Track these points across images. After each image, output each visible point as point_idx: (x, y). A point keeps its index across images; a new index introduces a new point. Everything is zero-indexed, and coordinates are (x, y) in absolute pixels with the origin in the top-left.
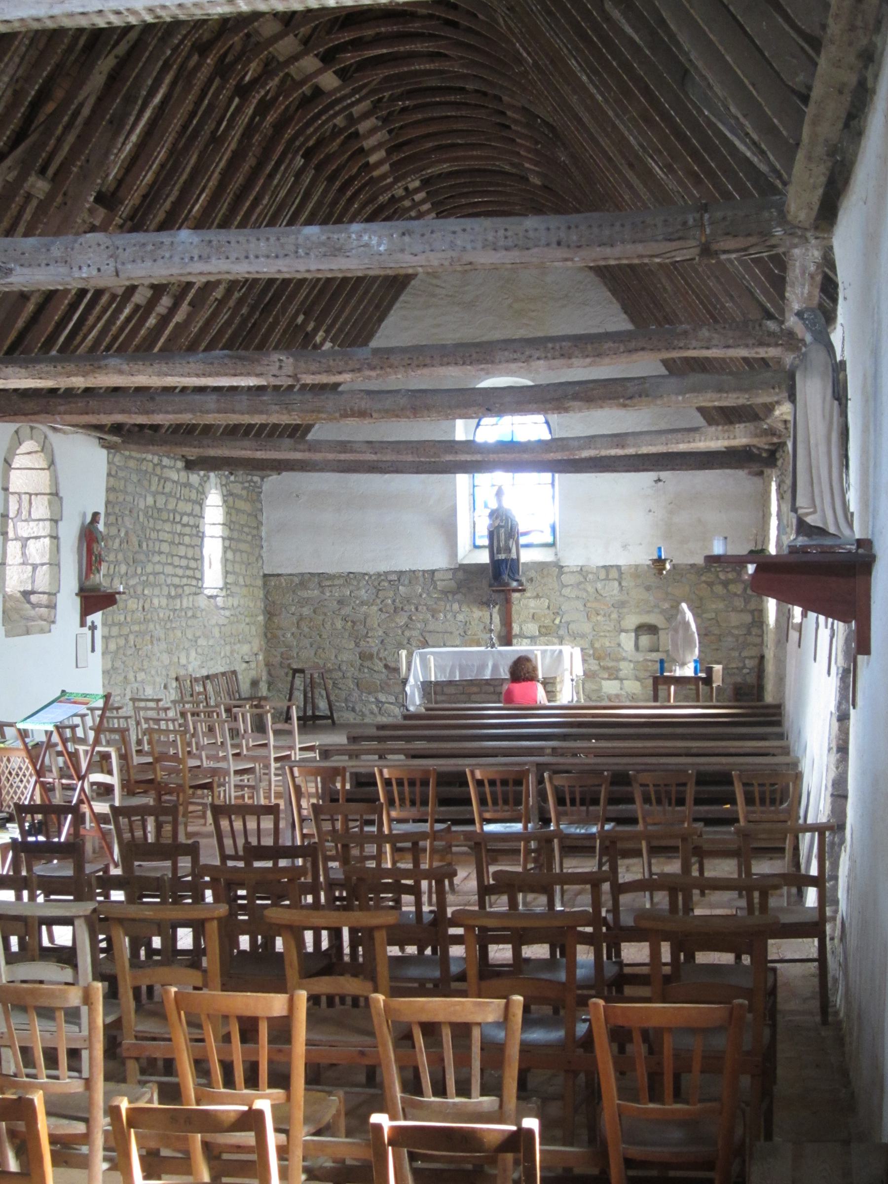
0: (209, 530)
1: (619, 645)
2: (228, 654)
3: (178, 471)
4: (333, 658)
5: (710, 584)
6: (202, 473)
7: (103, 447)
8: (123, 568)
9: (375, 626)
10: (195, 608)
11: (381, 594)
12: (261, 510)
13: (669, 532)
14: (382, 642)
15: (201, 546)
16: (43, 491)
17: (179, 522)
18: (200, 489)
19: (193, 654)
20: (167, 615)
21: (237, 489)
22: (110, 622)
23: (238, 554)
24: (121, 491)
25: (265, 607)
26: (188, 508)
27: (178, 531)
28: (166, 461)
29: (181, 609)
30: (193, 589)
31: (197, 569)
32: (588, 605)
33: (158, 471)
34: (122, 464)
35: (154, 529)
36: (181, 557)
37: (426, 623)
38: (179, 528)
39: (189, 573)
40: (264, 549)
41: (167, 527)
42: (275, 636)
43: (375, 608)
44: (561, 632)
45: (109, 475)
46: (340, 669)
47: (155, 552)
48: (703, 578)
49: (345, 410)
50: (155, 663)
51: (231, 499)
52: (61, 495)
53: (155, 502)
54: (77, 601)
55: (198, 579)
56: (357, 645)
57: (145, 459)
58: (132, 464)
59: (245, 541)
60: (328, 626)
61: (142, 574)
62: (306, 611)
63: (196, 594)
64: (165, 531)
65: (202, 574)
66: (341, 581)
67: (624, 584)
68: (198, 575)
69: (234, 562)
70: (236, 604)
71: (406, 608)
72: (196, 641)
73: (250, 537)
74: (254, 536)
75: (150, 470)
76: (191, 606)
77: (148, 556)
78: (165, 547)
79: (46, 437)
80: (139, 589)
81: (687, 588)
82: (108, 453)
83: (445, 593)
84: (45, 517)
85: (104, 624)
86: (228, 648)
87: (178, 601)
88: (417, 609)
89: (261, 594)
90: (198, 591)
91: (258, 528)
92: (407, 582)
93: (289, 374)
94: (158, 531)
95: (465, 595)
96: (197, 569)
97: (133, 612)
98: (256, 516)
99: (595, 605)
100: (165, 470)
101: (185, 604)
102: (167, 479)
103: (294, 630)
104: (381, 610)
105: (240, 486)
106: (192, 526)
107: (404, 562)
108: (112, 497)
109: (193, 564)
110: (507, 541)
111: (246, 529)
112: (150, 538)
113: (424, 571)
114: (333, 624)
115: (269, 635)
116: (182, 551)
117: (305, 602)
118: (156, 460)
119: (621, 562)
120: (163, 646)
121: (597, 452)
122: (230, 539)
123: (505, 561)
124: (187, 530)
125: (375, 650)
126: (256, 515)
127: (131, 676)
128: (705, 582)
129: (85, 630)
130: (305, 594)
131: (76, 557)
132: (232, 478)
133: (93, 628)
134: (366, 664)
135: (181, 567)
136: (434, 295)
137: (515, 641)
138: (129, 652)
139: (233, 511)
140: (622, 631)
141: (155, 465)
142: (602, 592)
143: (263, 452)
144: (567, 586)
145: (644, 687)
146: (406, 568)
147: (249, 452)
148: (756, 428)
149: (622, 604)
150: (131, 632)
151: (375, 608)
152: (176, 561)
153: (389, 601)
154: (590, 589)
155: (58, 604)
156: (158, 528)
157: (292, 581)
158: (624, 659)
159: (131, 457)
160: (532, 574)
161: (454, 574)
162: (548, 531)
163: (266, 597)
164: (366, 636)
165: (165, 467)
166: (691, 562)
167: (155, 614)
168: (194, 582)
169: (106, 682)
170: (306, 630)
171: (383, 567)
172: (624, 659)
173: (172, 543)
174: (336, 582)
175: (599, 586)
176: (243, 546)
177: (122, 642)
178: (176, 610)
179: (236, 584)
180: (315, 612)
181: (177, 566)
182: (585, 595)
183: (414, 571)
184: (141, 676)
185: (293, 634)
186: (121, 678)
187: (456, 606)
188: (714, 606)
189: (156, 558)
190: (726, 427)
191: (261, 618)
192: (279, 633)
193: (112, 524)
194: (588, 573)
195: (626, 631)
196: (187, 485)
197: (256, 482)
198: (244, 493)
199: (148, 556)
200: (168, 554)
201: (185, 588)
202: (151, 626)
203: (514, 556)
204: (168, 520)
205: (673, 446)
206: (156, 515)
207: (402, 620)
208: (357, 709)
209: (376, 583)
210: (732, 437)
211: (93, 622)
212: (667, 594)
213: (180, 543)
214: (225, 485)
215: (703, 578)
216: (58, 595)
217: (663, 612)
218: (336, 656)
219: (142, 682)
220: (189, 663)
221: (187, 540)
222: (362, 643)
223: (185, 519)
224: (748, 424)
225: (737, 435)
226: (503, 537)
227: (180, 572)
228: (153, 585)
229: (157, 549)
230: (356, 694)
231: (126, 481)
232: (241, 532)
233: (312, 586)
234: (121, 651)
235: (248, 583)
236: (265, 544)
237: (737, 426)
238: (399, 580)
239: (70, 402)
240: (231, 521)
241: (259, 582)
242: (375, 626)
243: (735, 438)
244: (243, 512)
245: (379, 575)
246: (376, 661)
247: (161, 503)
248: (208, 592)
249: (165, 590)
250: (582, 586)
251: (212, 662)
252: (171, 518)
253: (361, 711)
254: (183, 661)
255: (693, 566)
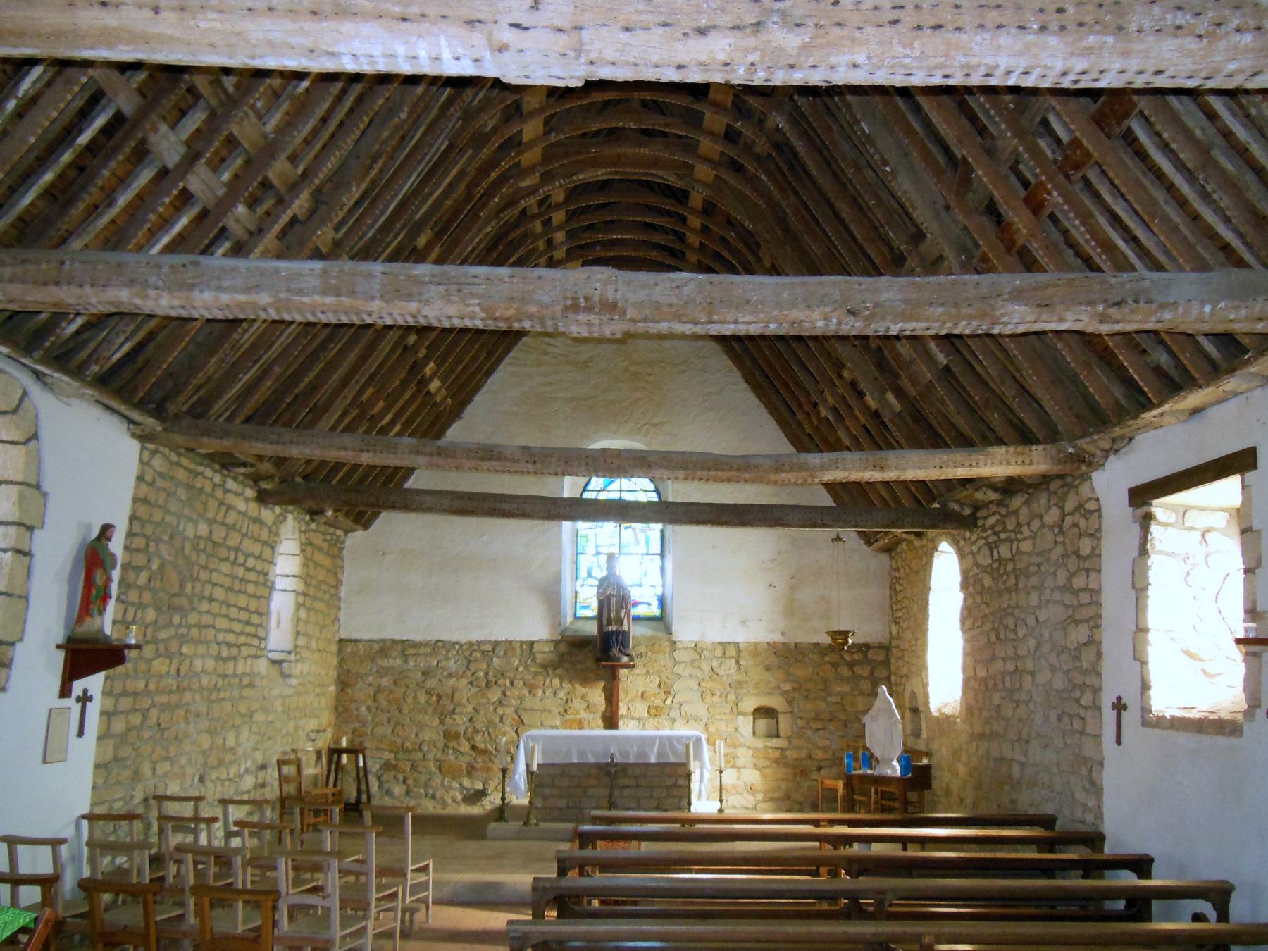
0: (281, 583)
1: (736, 729)
2: (291, 731)
3: (247, 500)
4: (413, 736)
5: (835, 666)
6: (278, 510)
7: (134, 435)
8: (151, 615)
9: (465, 701)
10: (252, 675)
11: (472, 666)
12: (342, 567)
13: (791, 609)
14: (471, 719)
15: (268, 599)
16: (12, 478)
17: (243, 565)
18: (274, 529)
19: (245, 732)
20: (213, 682)
21: (318, 539)
22: (118, 688)
23: (312, 614)
24: (159, 507)
25: (339, 676)
26: (256, 549)
27: (240, 576)
28: (231, 484)
29: (235, 675)
30: (253, 651)
31: (260, 625)
32: (703, 685)
33: (219, 493)
34: (163, 470)
35: (205, 568)
36: (240, 609)
37: (521, 699)
38: (241, 572)
39: (250, 629)
40: (342, 611)
41: (225, 567)
42: (346, 710)
43: (464, 682)
44: (673, 714)
45: (140, 478)
46: (420, 749)
47: (204, 597)
48: (827, 659)
49: (575, 299)
50: (187, 747)
51: (309, 549)
52: (46, 486)
53: (211, 532)
54: (60, 656)
55: (261, 639)
56: (442, 722)
57: (202, 474)
58: (181, 475)
59: (321, 600)
60: (409, 700)
61: (180, 625)
62: (385, 682)
63: (256, 657)
64: (221, 573)
65: (267, 634)
66: (428, 650)
67: (741, 662)
68: (261, 633)
69: (307, 622)
70: (305, 671)
71: (500, 682)
72: (251, 717)
73: (327, 597)
74: (332, 596)
75: (208, 489)
76: (248, 670)
77: (191, 601)
78: (219, 593)
79: (25, 394)
80: (174, 647)
81: (810, 669)
82: (143, 448)
83: (545, 667)
84: (9, 519)
85: (106, 693)
86: (292, 724)
87: (231, 664)
88: (512, 684)
89: (334, 661)
90: (260, 653)
91: (337, 587)
92: (502, 653)
93: (560, 23)
94: (211, 571)
95: (567, 670)
96: (260, 625)
97: (161, 676)
98: (336, 574)
99: (709, 685)
100: (229, 495)
101: (240, 669)
102: (229, 508)
103: (370, 702)
104: (471, 683)
105: (321, 537)
106: (259, 573)
107: (501, 631)
108: (143, 511)
109: (255, 619)
110: (618, 612)
111: (324, 587)
112: (197, 579)
113: (522, 642)
114: (415, 697)
115: (341, 709)
116: (242, 601)
117: (382, 673)
118: (217, 478)
119: (740, 638)
120: (204, 724)
121: (846, 474)
122: (305, 595)
123: (617, 633)
124: (252, 576)
125: (462, 729)
126: (336, 572)
127: (146, 770)
128: (829, 663)
129: (71, 703)
130: (386, 663)
131: (65, 588)
132: (313, 526)
133: (85, 698)
134: (451, 744)
135: (239, 621)
136: (547, 354)
137: (620, 723)
138: (147, 734)
139: (311, 565)
140: (740, 714)
141: (215, 486)
142: (718, 671)
143: (371, 454)
144: (679, 663)
145: (764, 776)
146: (502, 637)
147: (350, 453)
148: (1059, 451)
149: (740, 684)
150: (153, 705)
151: (464, 682)
152: (233, 613)
153: (481, 674)
154: (706, 668)
155: (16, 660)
156: (211, 566)
157: (371, 648)
158: (741, 745)
159: (178, 464)
160: (643, 649)
161: (555, 647)
162: (655, 604)
163: (340, 664)
164: (453, 712)
165: (229, 491)
166: (815, 641)
167: (195, 680)
168: (255, 642)
169: (100, 781)
170: (384, 703)
171: (475, 636)
172: (741, 745)
173: (230, 589)
174: (423, 650)
175: (715, 664)
176: (319, 605)
177: (136, 719)
178: (227, 676)
179: (308, 648)
180: (395, 683)
181: (233, 620)
182: (699, 674)
183: (511, 642)
184: (163, 767)
185: (368, 708)
186: (127, 773)
187: (556, 682)
188: (838, 689)
189: (205, 606)
190: (1019, 449)
191: (332, 688)
192: (353, 706)
193: (138, 550)
194: (703, 650)
195: (744, 714)
196: (257, 520)
197: (338, 537)
198: (325, 545)
199: (191, 601)
200: (222, 603)
201: (243, 648)
202: (188, 696)
203: (625, 628)
204: (226, 560)
205: (950, 470)
206: (209, 550)
207: (495, 695)
208: (438, 795)
209: (467, 653)
210: (1027, 461)
211: (85, 691)
212: (788, 674)
213: (240, 591)
214: (305, 532)
215: (827, 659)
216: (18, 645)
217: (783, 694)
218: (417, 735)
219: (166, 774)
220: (239, 745)
221: (251, 588)
222: (448, 720)
223: (251, 562)
224: (1048, 446)
225: (1035, 460)
226: (614, 607)
227: (237, 627)
228: (197, 642)
229: (207, 594)
230: (437, 779)
231: (168, 494)
232: (318, 588)
233: (394, 654)
234: (134, 733)
235: (321, 647)
236: (343, 606)
237: (1034, 447)
238: (493, 650)
239: (24, 261)
240: (308, 575)
241: (334, 648)
242: (465, 701)
243: (1031, 463)
244: (322, 566)
245: (471, 644)
246: (463, 741)
247: (219, 533)
248: (273, 656)
249: (214, 649)
250: (696, 664)
251: (270, 743)
252: (232, 557)
253: (442, 798)
254: (231, 742)
255: (816, 645)
